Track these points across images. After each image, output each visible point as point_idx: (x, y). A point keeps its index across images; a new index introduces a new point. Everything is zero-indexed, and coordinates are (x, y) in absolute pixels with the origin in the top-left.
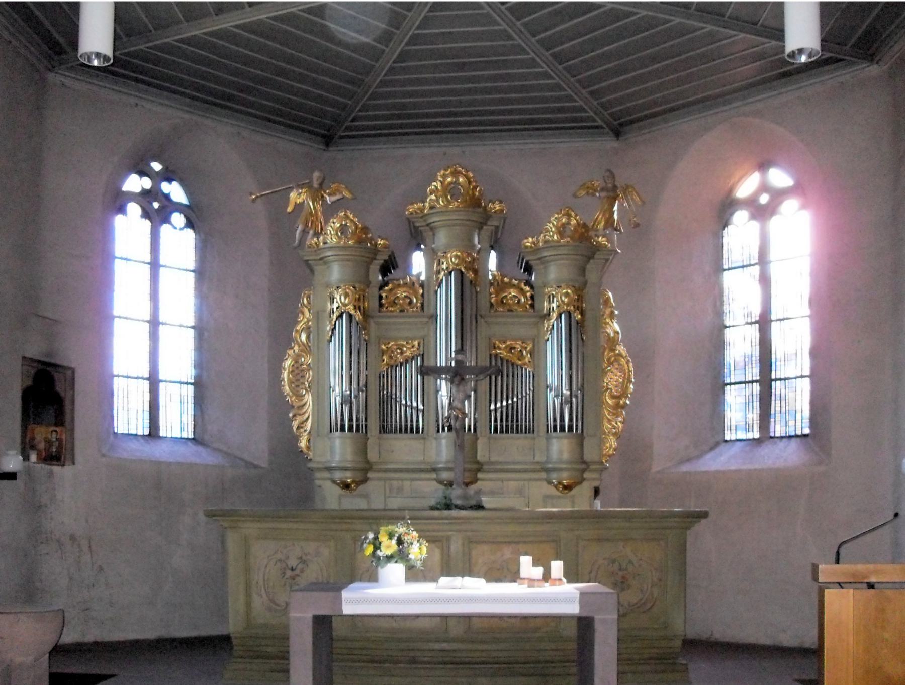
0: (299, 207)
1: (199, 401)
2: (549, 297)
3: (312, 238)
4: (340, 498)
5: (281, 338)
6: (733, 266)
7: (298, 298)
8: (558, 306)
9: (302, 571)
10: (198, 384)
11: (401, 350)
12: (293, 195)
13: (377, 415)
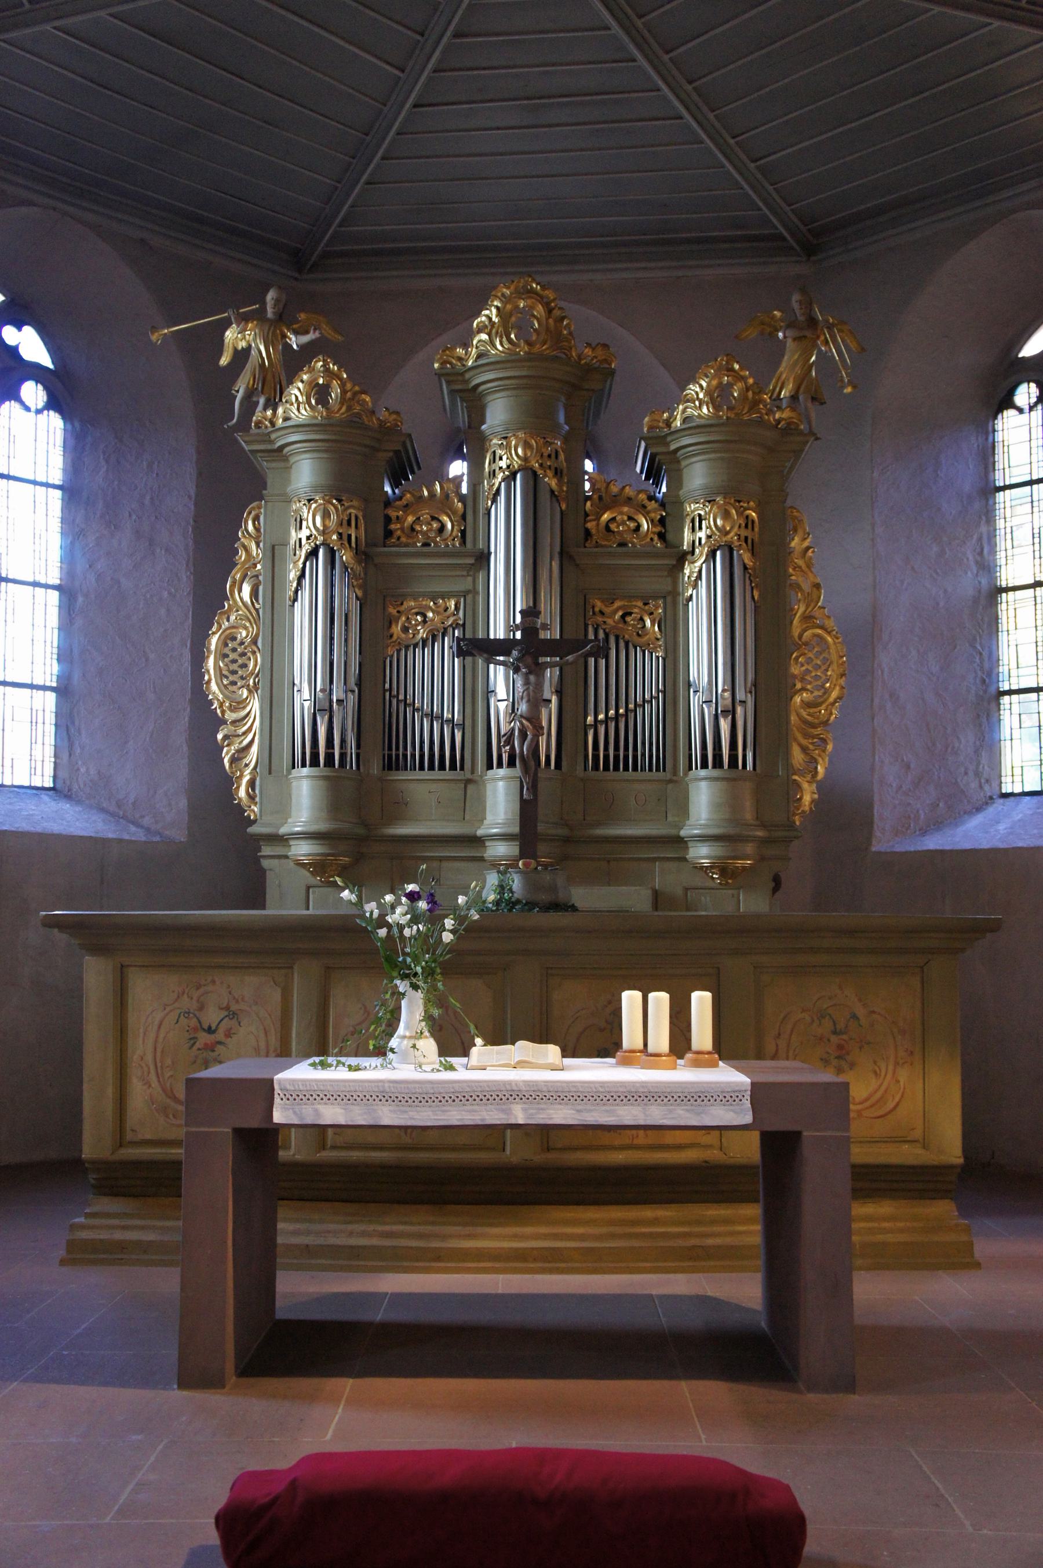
0: (242, 356)
1: (66, 724)
2: (693, 521)
3: (265, 409)
4: (308, 888)
5: (210, 601)
6: (1014, 481)
7: (237, 523)
8: (709, 537)
9: (228, 1034)
10: (63, 690)
11: (424, 616)
12: (230, 334)
13: (374, 747)
